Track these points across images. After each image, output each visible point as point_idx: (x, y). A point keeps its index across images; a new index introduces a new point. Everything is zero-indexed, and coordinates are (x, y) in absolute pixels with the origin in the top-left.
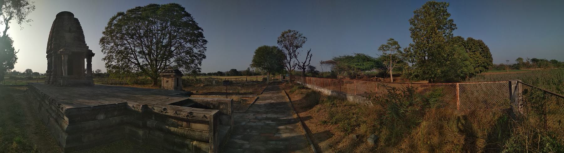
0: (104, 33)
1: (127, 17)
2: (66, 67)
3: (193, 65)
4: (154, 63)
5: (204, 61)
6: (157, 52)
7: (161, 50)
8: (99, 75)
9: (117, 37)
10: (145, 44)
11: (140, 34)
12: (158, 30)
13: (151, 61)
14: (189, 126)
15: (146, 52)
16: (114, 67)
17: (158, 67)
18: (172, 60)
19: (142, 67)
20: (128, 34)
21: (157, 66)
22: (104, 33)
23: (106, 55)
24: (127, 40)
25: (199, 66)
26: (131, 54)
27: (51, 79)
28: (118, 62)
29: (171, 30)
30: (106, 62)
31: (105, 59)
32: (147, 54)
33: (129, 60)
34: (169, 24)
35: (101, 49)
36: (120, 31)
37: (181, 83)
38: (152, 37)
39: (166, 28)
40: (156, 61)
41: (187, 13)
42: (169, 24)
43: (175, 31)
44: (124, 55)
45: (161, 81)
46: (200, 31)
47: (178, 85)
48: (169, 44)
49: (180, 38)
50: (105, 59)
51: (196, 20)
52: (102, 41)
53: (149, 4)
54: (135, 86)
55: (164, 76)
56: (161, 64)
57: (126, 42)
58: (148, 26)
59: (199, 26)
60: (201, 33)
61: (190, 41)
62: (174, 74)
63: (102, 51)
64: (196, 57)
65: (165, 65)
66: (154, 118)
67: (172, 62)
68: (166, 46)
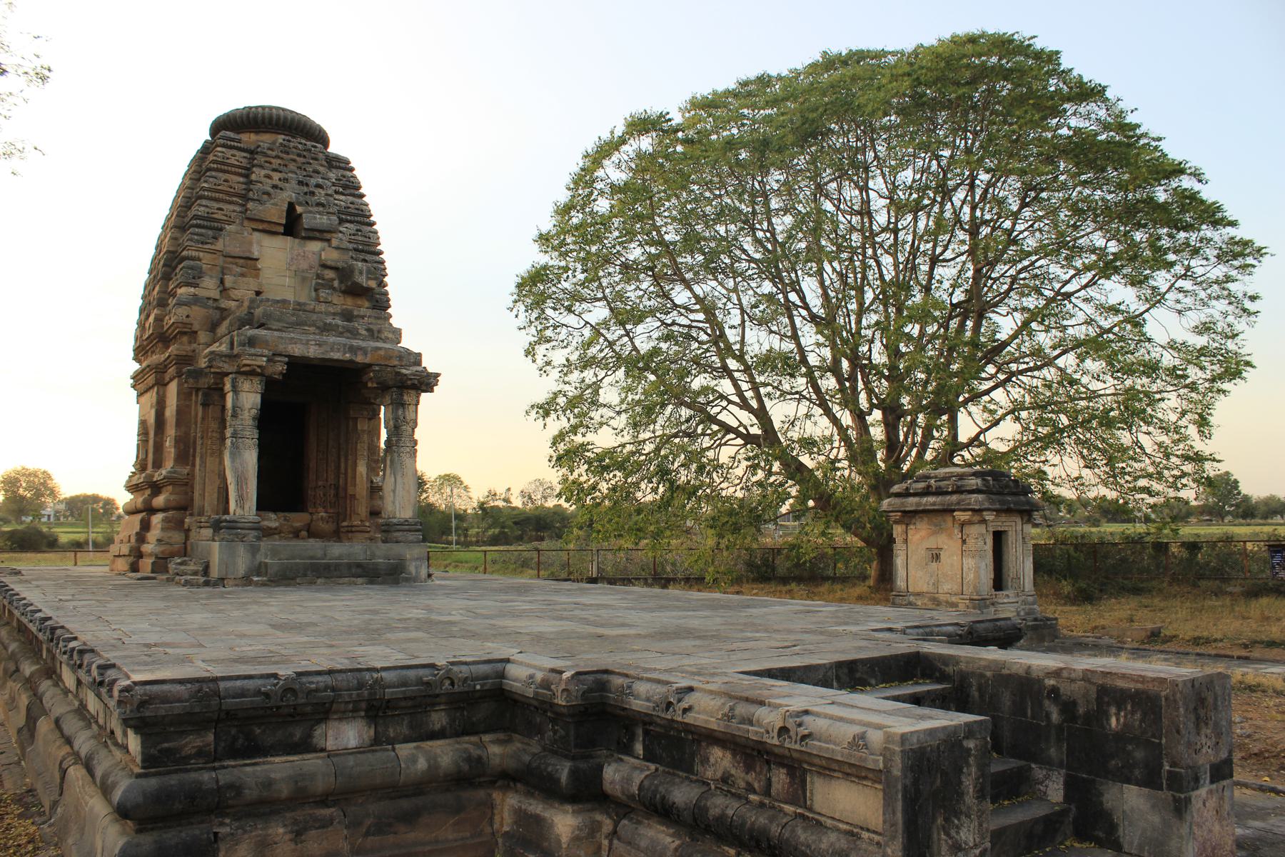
0: (544, 239)
1: (687, 142)
9: (626, 267)
14: (798, 794)
16: (604, 463)
22: (544, 239)
25: (1199, 445)
27: (154, 534)
30: (557, 424)
31: (545, 409)
35: (528, 337)
41: (1080, 83)
59: (1174, 151)
63: (530, 352)
66: (639, 748)
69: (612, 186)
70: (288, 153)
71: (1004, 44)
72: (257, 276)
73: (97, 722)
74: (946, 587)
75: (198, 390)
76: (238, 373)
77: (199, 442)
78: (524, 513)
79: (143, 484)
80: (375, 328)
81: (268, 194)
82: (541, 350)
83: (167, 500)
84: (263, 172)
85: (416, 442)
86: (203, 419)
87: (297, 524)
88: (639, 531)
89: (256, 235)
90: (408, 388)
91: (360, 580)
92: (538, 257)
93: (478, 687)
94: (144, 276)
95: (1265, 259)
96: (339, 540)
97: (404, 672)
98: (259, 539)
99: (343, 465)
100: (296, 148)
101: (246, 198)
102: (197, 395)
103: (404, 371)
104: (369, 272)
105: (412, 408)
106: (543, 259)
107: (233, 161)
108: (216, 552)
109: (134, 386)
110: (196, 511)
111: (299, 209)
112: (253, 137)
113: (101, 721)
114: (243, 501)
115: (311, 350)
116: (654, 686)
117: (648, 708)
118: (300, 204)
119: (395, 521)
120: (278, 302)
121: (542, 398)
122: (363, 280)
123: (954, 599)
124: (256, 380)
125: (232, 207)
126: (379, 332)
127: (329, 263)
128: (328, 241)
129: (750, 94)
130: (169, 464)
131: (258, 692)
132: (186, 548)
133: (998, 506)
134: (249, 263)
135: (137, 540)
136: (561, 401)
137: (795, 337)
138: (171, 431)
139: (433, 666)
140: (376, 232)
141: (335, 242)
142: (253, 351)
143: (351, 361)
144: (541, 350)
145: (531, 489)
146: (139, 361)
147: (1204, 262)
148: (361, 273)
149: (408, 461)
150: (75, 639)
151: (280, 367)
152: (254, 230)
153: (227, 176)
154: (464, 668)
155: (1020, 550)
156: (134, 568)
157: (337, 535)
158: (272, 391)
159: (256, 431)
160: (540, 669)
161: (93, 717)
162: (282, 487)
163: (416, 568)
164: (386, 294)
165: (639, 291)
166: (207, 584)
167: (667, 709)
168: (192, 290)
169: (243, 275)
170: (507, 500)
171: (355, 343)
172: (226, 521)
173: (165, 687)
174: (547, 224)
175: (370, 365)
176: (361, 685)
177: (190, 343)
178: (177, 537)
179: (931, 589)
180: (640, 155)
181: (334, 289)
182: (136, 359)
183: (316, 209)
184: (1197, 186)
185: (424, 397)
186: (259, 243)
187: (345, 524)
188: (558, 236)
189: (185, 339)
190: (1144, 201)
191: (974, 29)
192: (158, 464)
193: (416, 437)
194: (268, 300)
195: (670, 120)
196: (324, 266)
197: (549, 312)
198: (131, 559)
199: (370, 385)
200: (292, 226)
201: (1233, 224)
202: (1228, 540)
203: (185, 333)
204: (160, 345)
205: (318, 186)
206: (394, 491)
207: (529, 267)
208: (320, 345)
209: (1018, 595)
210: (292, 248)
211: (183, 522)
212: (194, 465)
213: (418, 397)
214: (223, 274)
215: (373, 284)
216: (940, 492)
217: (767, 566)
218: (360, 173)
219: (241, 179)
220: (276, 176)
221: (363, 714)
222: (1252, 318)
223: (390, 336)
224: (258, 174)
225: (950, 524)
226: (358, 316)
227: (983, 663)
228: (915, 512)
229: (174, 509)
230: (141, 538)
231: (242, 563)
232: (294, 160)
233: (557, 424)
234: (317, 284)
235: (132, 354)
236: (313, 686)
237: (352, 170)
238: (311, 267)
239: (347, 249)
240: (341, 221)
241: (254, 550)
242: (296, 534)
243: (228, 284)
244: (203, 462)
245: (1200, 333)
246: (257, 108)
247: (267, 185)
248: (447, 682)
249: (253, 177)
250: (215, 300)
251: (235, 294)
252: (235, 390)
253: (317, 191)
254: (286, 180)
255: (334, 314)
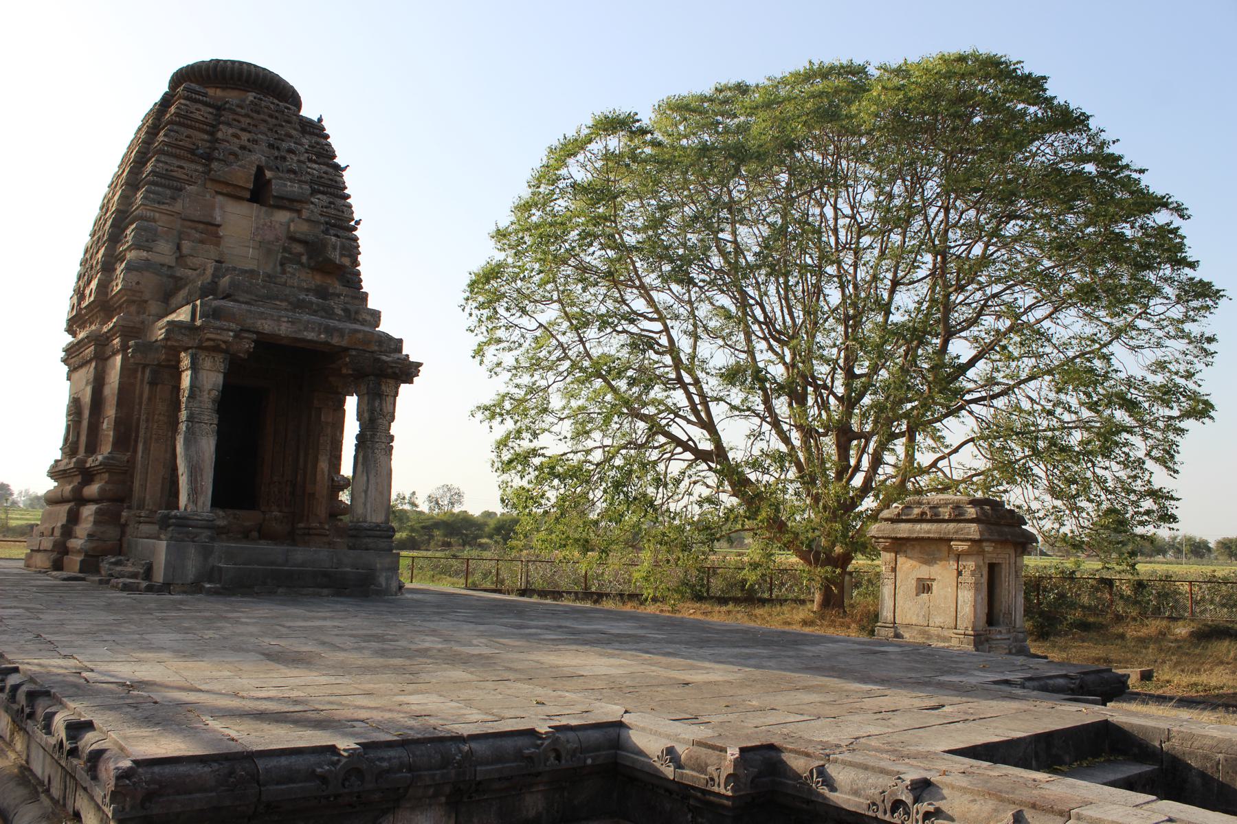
0: (501, 235)
2: (208, 446)
3: (1111, 471)
4: (829, 444)
5: (1195, 439)
6: (850, 375)
7: (880, 357)
8: (455, 531)
9: (583, 269)
10: (769, 322)
11: (739, 250)
12: (861, 230)
13: (808, 433)
15: (778, 371)
16: (551, 471)
17: (858, 481)
18: (956, 429)
19: (733, 476)
20: (656, 252)
21: (845, 471)
23: (500, 384)
24: (645, 291)
25: (1160, 478)
26: (668, 385)
28: (582, 433)
29: (948, 226)
30: (502, 428)
31: (492, 411)
32: (781, 389)
33: (655, 428)
34: (932, 187)
35: (473, 341)
36: (602, 229)
37: (1014, 599)
38: (819, 271)
39: (911, 212)
40: (845, 436)
42: (932, 187)
43: (974, 231)
44: (625, 389)
45: (875, 580)
46: (1161, 217)
47: (991, 620)
48: (939, 321)
49: (1012, 280)
50: (492, 411)
51: (1129, 151)
52: (486, 286)
53: (801, 66)
54: (690, 612)
55: (899, 545)
56: (877, 461)
57: (639, 305)
58: (791, 201)
59: (1154, 183)
60: (1166, 232)
61: (1086, 295)
62: (973, 530)
63: (479, 352)
64: (1131, 406)
65: (909, 469)
67: (957, 449)
68: (914, 334)
69: (574, 185)
70: (259, 113)
71: (994, 67)
72: (218, 244)
73: (47, 791)
74: (938, 620)
75: (145, 367)
76: (200, 348)
77: (143, 425)
78: (432, 518)
79: (73, 470)
80: (352, 308)
81: (235, 155)
82: (490, 351)
83: (102, 490)
84: (231, 131)
85: (392, 438)
86: (150, 399)
87: (247, 524)
88: (586, 546)
89: (219, 198)
90: (387, 376)
91: (325, 591)
92: (490, 253)
93: (589, 761)
94: (85, 239)
95: (1222, 302)
96: (294, 542)
97: (499, 742)
98: (212, 539)
99: (301, 460)
100: (267, 107)
101: (209, 158)
102: (143, 373)
103: (384, 358)
104: (343, 247)
105: (390, 399)
106: (500, 256)
107: (197, 116)
108: (160, 552)
109: (65, 361)
110: (135, 503)
111: (268, 174)
112: (219, 93)
113: (56, 792)
114: (193, 493)
115: (283, 328)
116: (862, 774)
117: (859, 805)
118: (270, 169)
119: (365, 525)
120: (246, 271)
121: (488, 399)
122: (336, 256)
123: (946, 633)
124: (219, 357)
125: (193, 166)
126: (357, 313)
127: (298, 235)
128: (299, 211)
129: (726, 101)
130: (106, 449)
131: (312, 775)
132: (121, 545)
133: (996, 537)
134: (210, 230)
135: (62, 534)
136: (507, 405)
137: (751, 352)
138: (110, 412)
139: (532, 733)
140: (350, 206)
141: (305, 214)
142: (218, 323)
143: (326, 343)
144: (490, 351)
145: (438, 494)
146: (74, 334)
147: (1165, 301)
148: (334, 248)
149: (382, 458)
150: (16, 670)
151: (247, 345)
152: (218, 193)
153: (190, 132)
154: (571, 735)
155: (1012, 583)
156: (58, 565)
157: (292, 538)
158: (235, 369)
159: (215, 416)
160: (685, 742)
161: (41, 783)
162: (236, 483)
163: (387, 579)
164: (358, 273)
165: (596, 300)
166: (150, 589)
167: (893, 811)
168: (145, 254)
169: (202, 242)
170: (414, 505)
171: (333, 323)
172: (175, 517)
173: (182, 769)
174: (505, 219)
175: (346, 349)
176: (446, 762)
177: (138, 313)
178: (112, 532)
179: (922, 622)
180: (608, 156)
181: (302, 265)
182: (70, 330)
183: (287, 176)
184: (1177, 222)
185: (404, 388)
186: (222, 208)
187: (301, 525)
188: (517, 234)
189: (133, 309)
190: (1113, 234)
191: (965, 48)
192: (92, 448)
193: (392, 432)
194: (234, 269)
195: (638, 121)
196: (292, 238)
197: (501, 311)
198: (54, 555)
199: (344, 371)
200: (259, 193)
201: (1192, 265)
202: (1168, 578)
203: (134, 302)
204: (102, 314)
205: (290, 151)
206: (366, 492)
207: (483, 263)
208: (292, 323)
209: (1009, 632)
210: (258, 217)
211: (119, 516)
212: (135, 451)
213: (397, 388)
214: (181, 239)
215: (346, 261)
216: (936, 519)
217: (702, 586)
218: (336, 141)
219: (206, 137)
220: (245, 136)
221: (443, 799)
222: (1209, 359)
223: (368, 318)
224: (224, 132)
225: (945, 554)
226: (333, 294)
227: (1209, 742)
228: (907, 539)
229: (109, 500)
230: (68, 531)
231: (192, 565)
232: (265, 121)
233: (502, 428)
234: (283, 257)
235: (64, 325)
236: (385, 764)
237: (327, 137)
238: (278, 239)
239: (318, 222)
240: (314, 192)
241: (206, 552)
242: (246, 535)
243: (185, 250)
244: (147, 450)
245: (1154, 372)
246: (225, 61)
247: (231, 159)
248: (552, 755)
249: (220, 135)
250: (170, 267)
251: (190, 261)
252: (194, 367)
253: (288, 156)
254: (255, 142)
255: (308, 290)
